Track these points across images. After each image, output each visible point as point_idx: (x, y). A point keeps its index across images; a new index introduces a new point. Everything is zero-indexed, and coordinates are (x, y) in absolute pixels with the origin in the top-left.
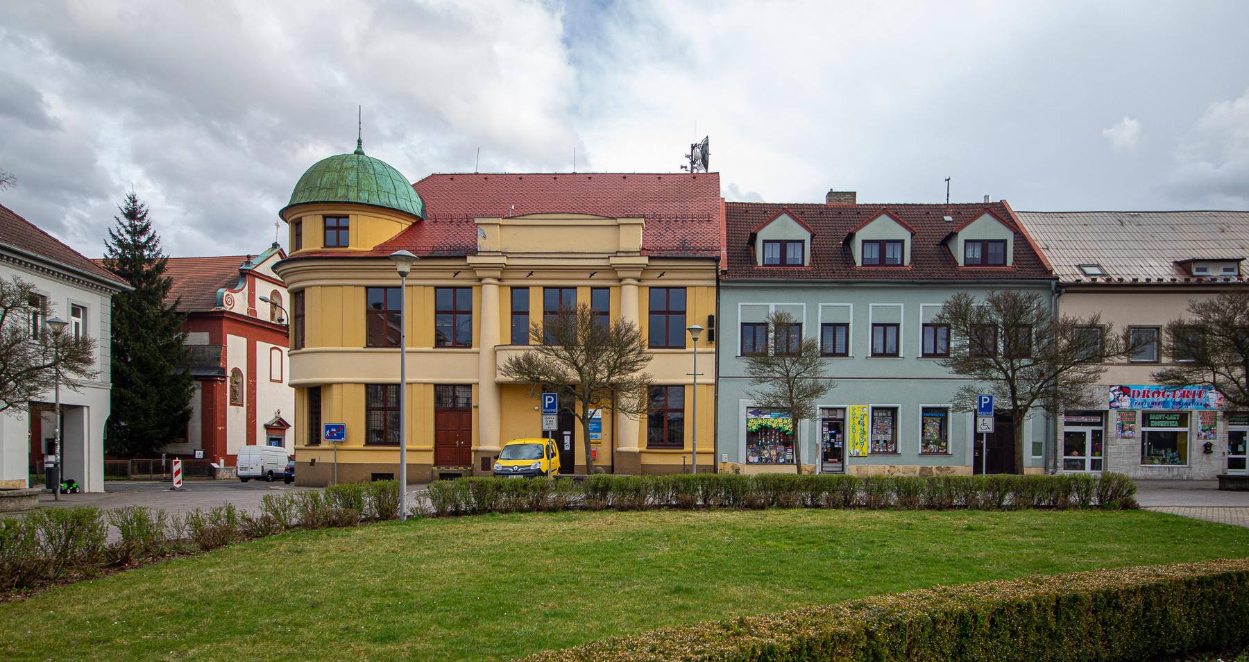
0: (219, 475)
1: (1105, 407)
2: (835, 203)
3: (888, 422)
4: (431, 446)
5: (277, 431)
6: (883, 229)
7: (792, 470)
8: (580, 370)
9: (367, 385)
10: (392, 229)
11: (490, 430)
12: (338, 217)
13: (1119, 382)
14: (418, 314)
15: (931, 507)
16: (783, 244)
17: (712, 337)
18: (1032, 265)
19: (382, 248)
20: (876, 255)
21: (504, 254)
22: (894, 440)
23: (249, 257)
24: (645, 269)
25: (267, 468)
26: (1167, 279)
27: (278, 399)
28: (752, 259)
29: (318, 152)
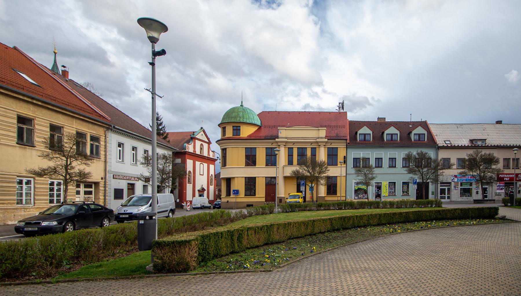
0: (184, 208)
1: (451, 181)
2: (379, 121)
3: (393, 186)
4: (264, 196)
5: (202, 192)
6: (392, 130)
7: (367, 200)
8: (310, 173)
9: (245, 178)
10: (253, 129)
11: (283, 191)
12: (237, 126)
13: (447, 175)
14: (261, 156)
15: (397, 208)
16: (365, 135)
17: (345, 162)
18: (432, 143)
19: (250, 136)
20: (390, 138)
21: (286, 138)
22: (395, 191)
23: (194, 132)
24: (326, 142)
25: (202, 204)
26: (466, 145)
27: (201, 181)
28: (356, 139)
29: (229, 106)
